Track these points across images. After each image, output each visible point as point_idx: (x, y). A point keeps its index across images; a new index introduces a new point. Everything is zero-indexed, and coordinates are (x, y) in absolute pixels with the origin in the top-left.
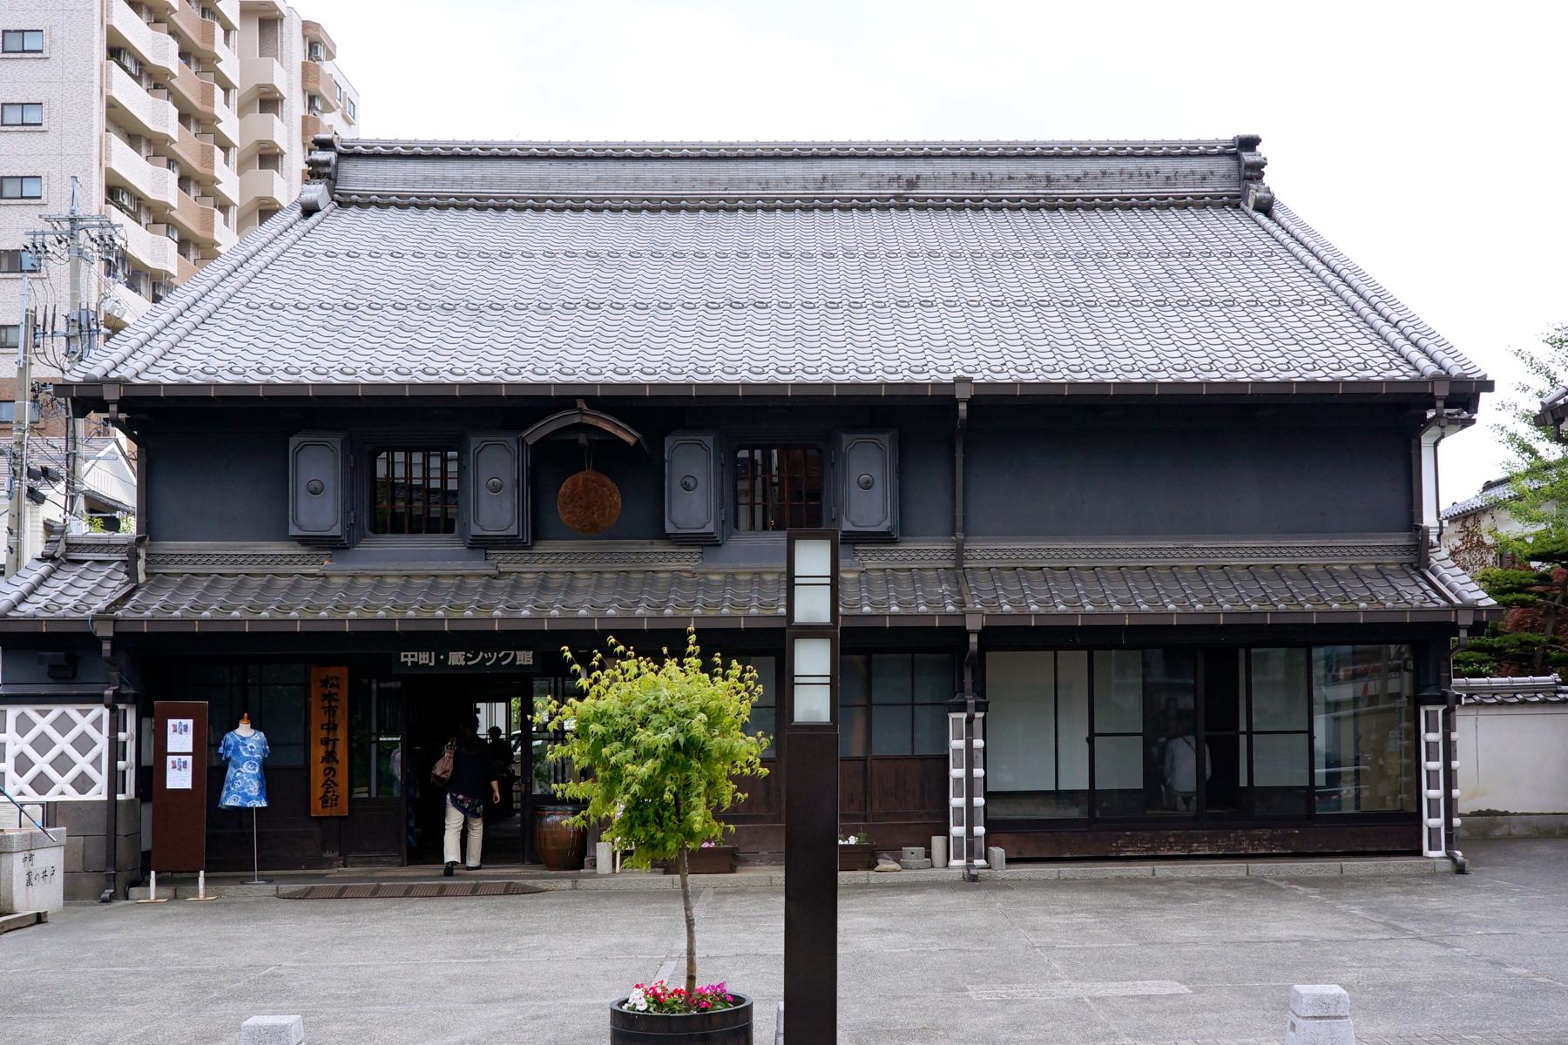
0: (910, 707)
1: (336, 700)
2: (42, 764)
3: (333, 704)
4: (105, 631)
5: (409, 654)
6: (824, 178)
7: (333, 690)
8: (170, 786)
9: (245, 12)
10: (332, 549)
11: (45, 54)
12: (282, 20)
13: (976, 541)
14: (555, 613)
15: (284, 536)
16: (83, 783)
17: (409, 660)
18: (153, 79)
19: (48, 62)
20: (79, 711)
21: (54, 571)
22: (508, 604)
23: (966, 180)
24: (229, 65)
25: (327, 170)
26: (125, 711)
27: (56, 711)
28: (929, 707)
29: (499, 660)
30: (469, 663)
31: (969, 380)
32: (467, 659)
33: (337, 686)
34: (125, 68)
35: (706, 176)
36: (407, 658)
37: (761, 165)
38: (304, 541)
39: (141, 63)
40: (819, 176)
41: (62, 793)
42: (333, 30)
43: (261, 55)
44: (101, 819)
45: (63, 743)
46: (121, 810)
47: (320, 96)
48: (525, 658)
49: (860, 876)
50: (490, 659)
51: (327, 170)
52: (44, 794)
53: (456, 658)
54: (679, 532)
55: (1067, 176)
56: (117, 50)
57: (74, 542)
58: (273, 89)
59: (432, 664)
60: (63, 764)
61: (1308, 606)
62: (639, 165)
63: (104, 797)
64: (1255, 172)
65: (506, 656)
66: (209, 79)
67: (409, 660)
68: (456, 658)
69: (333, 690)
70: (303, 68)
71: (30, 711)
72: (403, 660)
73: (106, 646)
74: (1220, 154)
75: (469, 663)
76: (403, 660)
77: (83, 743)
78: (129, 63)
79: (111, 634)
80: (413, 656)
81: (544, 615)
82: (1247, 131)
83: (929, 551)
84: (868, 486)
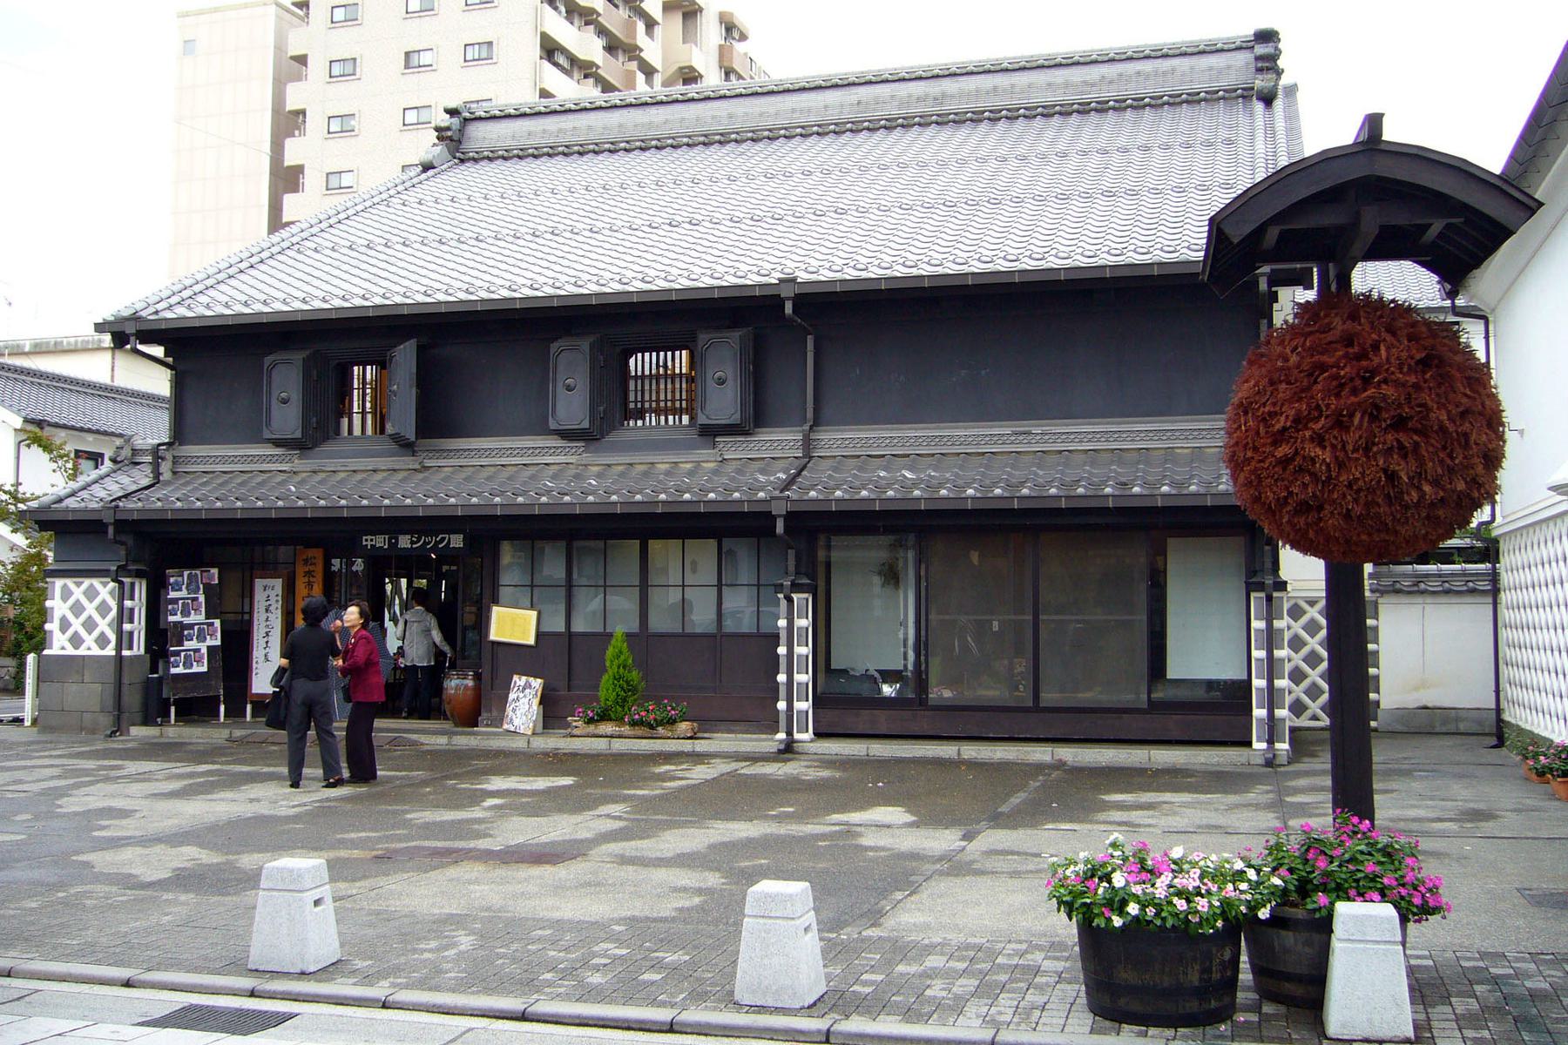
0: (756, 588)
1: (313, 576)
2: (77, 625)
3: (311, 579)
4: (779, 509)
5: (369, 537)
6: (859, 103)
7: (311, 568)
8: (494, 636)
9: (667, 8)
10: (300, 449)
11: (495, 60)
12: (701, 12)
13: (826, 431)
14: (1025, 491)
15: (257, 439)
16: (102, 641)
17: (369, 543)
18: (582, 69)
19: (495, 67)
20: (101, 582)
21: (115, 472)
22: (955, 484)
23: (987, 93)
24: (652, 51)
25: (449, 133)
26: (133, 585)
27: (87, 582)
28: (746, 588)
29: (437, 543)
30: (414, 546)
31: (793, 280)
32: (412, 543)
33: (314, 564)
34: (556, 65)
35: (758, 110)
36: (368, 541)
37: (805, 96)
38: (278, 443)
39: (573, 60)
40: (822, 104)
41: (89, 649)
42: (743, 19)
43: (684, 43)
44: (111, 669)
45: (90, 609)
46: (125, 664)
47: (734, 71)
48: (457, 541)
49: (432, 736)
50: (429, 543)
51: (449, 133)
52: (103, 649)
53: (404, 542)
54: (561, 428)
55: (1084, 82)
56: (550, 50)
57: (139, 447)
58: (692, 69)
59: (386, 547)
60: (90, 625)
61: (199, 504)
62: (701, 106)
63: (113, 653)
64: (1269, 64)
65: (444, 539)
66: (634, 65)
67: (369, 543)
68: (404, 542)
69: (311, 568)
70: (720, 50)
71: (70, 582)
72: (364, 543)
73: (111, 530)
74: (1239, 48)
75: (414, 546)
76: (364, 543)
77: (103, 609)
78: (561, 60)
79: (112, 521)
80: (372, 540)
81: (1157, 492)
82: (1264, 25)
83: (779, 442)
84: (285, 401)
